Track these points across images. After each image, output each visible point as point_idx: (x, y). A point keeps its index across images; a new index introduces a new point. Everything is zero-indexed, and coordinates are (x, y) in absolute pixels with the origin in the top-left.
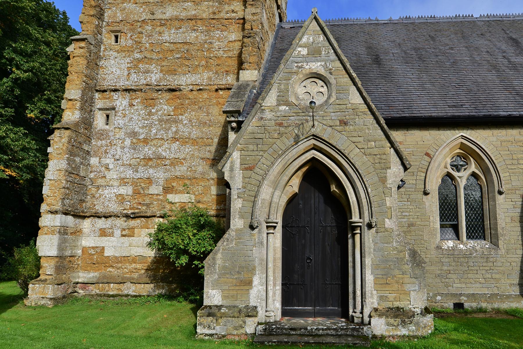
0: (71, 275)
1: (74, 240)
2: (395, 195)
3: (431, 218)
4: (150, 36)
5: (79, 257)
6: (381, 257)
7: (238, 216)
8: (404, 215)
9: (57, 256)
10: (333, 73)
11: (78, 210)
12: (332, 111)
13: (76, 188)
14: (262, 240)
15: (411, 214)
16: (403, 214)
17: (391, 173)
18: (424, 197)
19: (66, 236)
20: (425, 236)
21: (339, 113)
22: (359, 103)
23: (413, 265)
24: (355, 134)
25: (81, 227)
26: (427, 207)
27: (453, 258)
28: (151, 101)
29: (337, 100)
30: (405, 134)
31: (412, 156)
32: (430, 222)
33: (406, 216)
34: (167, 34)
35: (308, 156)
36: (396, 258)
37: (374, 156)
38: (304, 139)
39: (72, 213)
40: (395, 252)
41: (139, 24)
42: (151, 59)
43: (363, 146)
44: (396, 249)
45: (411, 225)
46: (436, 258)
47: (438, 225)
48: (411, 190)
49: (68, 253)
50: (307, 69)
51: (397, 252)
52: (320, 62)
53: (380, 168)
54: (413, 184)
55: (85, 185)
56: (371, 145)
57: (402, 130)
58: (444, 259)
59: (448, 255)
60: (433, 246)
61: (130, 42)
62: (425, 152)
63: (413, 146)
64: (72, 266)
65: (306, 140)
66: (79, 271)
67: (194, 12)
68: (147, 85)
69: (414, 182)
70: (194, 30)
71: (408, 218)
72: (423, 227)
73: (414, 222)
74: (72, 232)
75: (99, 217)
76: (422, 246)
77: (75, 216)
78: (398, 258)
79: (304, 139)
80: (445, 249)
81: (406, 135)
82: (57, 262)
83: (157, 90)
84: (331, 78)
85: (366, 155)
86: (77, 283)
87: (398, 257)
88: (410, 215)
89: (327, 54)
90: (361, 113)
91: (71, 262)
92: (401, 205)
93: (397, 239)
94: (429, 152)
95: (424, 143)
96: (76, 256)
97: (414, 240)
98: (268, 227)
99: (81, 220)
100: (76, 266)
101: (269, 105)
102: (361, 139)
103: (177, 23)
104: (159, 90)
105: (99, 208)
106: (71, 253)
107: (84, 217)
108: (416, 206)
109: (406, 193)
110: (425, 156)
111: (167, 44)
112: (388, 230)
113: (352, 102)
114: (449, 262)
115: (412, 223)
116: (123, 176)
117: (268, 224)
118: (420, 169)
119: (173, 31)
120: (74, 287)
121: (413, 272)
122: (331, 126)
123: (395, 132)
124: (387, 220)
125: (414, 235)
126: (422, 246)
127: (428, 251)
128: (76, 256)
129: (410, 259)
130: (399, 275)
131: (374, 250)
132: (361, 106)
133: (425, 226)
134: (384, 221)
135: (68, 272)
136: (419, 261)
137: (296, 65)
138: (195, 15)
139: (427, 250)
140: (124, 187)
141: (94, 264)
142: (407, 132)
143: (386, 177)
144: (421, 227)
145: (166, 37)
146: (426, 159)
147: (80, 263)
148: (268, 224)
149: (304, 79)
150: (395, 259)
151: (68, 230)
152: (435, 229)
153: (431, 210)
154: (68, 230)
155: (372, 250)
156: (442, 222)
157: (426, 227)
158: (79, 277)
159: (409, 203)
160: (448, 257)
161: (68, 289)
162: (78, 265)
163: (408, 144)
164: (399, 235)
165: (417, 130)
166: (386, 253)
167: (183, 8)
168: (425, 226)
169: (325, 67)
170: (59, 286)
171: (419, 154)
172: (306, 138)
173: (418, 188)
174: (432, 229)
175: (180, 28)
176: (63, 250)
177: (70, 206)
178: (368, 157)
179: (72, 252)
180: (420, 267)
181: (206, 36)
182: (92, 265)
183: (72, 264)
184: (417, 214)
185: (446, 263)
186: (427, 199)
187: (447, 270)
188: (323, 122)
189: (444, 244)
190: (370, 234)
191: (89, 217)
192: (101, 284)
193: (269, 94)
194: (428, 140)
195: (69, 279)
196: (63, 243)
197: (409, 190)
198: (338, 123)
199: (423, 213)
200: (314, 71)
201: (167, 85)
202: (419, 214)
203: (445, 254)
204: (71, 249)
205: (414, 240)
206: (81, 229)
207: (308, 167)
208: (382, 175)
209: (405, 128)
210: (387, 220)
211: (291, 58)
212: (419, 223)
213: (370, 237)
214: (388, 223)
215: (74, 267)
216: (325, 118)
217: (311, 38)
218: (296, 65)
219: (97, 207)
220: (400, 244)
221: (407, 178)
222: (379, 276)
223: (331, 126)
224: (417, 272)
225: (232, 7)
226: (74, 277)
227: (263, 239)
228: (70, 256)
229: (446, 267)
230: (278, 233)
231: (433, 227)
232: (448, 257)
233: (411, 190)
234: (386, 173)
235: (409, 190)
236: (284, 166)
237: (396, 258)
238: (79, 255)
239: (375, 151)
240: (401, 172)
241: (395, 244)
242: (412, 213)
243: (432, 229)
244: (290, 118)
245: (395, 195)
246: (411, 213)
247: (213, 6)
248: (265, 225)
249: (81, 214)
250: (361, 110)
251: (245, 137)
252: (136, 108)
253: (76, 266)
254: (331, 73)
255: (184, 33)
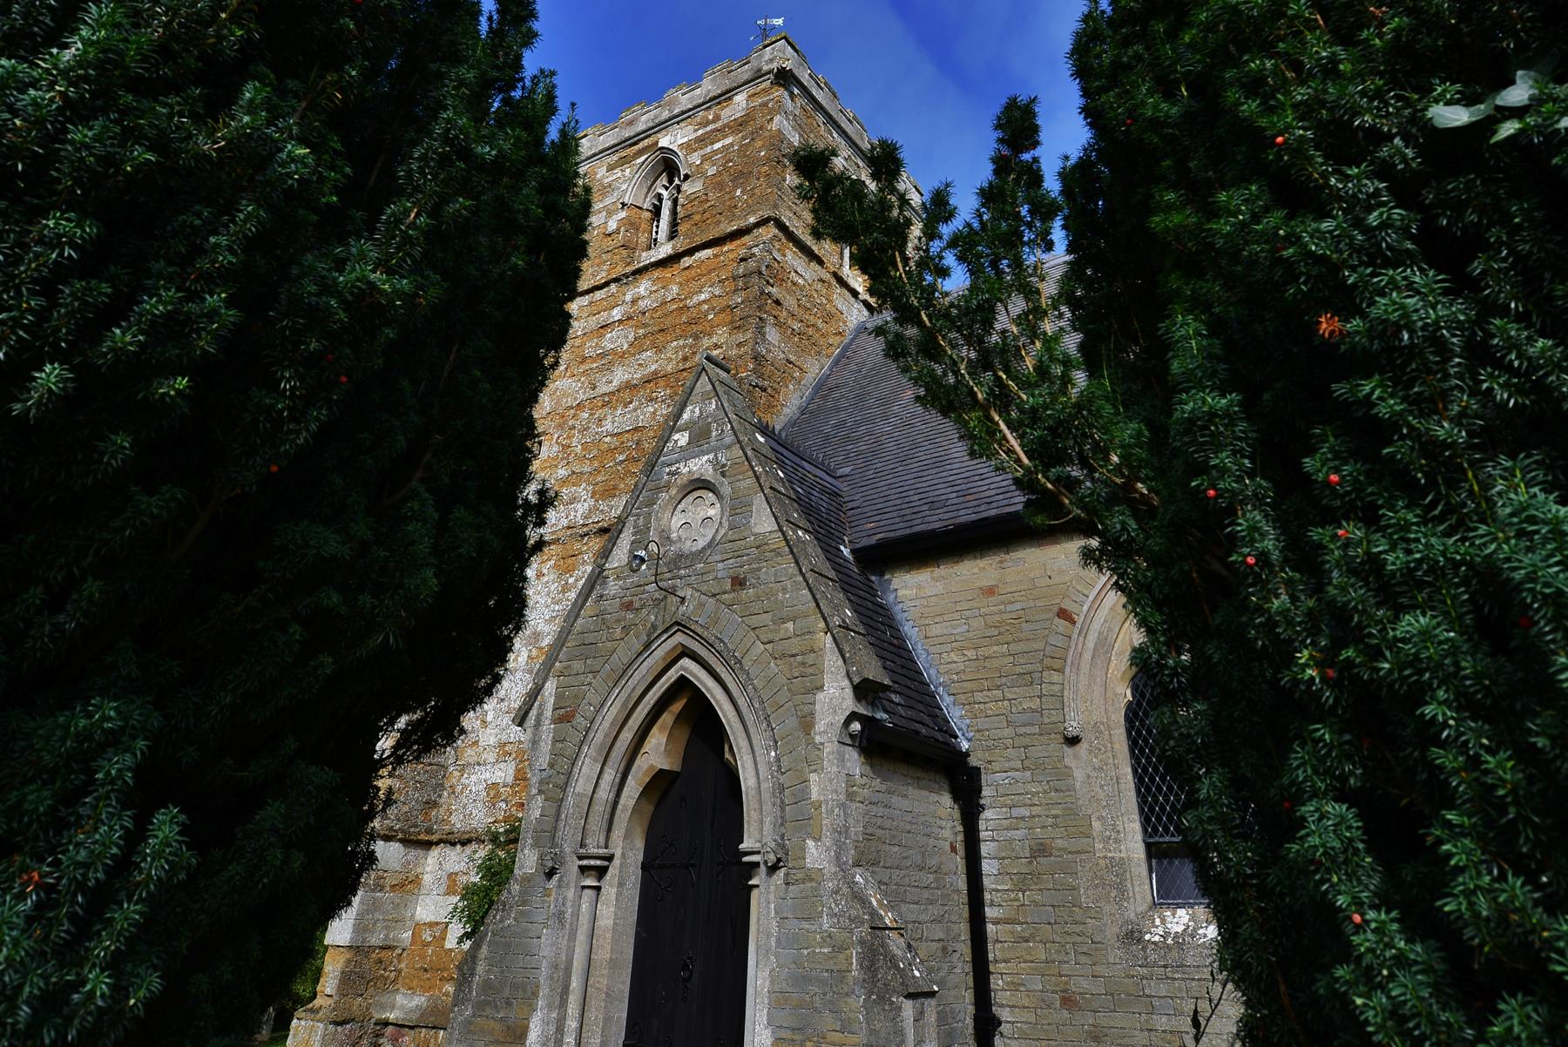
0: (376, 998)
1: (398, 905)
2: (833, 764)
3: (1096, 824)
4: (585, 430)
5: (404, 950)
6: (794, 966)
7: (530, 841)
8: (1016, 818)
9: (351, 947)
10: (727, 474)
11: (416, 826)
12: (718, 558)
13: (419, 774)
14: (562, 909)
15: (1036, 810)
16: (1016, 812)
17: (824, 703)
18: (1068, 750)
19: (378, 894)
20: (1082, 890)
21: (731, 561)
22: (769, 529)
23: (870, 997)
24: (756, 607)
25: (419, 870)
26: (1078, 785)
27: (1183, 979)
28: (569, 561)
29: (730, 532)
30: (1001, 562)
31: (1024, 625)
32: (1093, 839)
33: (1023, 818)
34: (609, 418)
35: (672, 675)
36: (827, 971)
37: (792, 659)
38: (660, 635)
39: (400, 836)
40: (826, 951)
41: (572, 411)
42: (581, 473)
43: (770, 636)
44: (828, 939)
45: (1040, 850)
46: (1127, 980)
47: (1133, 846)
48: (1028, 730)
49: (376, 939)
50: (684, 474)
51: (830, 949)
52: (708, 454)
53: (803, 691)
54: (1034, 711)
55: (443, 766)
56: (787, 630)
57: (995, 554)
58: (1152, 984)
59: (1165, 966)
60: (1112, 931)
61: (555, 449)
62: (1056, 609)
63: (1023, 593)
64: (382, 976)
65: (665, 636)
66: (398, 989)
67: (653, 367)
68: (569, 528)
69: (1035, 704)
70: (651, 400)
71: (1027, 825)
72: (1074, 856)
73: (1048, 841)
74: (396, 882)
75: (453, 844)
76: (1078, 928)
77: (408, 842)
78: (832, 971)
79: (660, 635)
80: (1153, 943)
81: (1004, 565)
82: (349, 961)
83: (581, 536)
84: (722, 483)
85: (776, 658)
86: (386, 1023)
87: (832, 967)
88: (1034, 817)
89: (720, 435)
90: (773, 554)
91: (381, 962)
92: (1006, 781)
93: (833, 905)
94: (1068, 605)
95: (1051, 582)
96: (396, 947)
97: (1053, 906)
98: (583, 869)
99: (421, 852)
100: (393, 974)
101: (616, 565)
102: (767, 619)
103: (626, 395)
104: (585, 535)
105: (457, 822)
106: (384, 940)
107: (428, 845)
108: (1048, 782)
109: (1018, 741)
110: (1057, 621)
111: (607, 439)
112: (813, 876)
113: (756, 530)
114: (1171, 998)
115: (1042, 844)
116: (504, 738)
117: (585, 862)
118: (1047, 661)
119: (619, 412)
120: (377, 1036)
121: (868, 1023)
122: (714, 595)
123: (979, 561)
124: (810, 843)
125: (1051, 886)
126: (1078, 928)
127: (1097, 949)
128: (396, 947)
129: (861, 977)
130: (835, 1033)
131: (778, 941)
132: (773, 536)
133: (1079, 852)
134: (803, 849)
135: (371, 990)
136: (885, 984)
137: (667, 470)
138: (655, 372)
139: (1093, 946)
140: (502, 765)
141: (426, 970)
142: (1007, 557)
143: (812, 714)
144: (1070, 856)
145: (608, 426)
146: (1061, 629)
147: (403, 966)
148: (585, 862)
149: (681, 496)
150: (825, 974)
151: (385, 878)
152: (1119, 867)
153: (1093, 794)
154: (385, 878)
155: (773, 941)
156: (1151, 836)
157: (1083, 857)
158: (393, 1007)
159: (1028, 773)
160: (1167, 978)
161: (360, 1037)
162: (399, 971)
163: (1009, 590)
164: (837, 893)
165: (1031, 547)
166: (805, 952)
167: (639, 365)
168: (1079, 852)
169: (716, 464)
170: (339, 1029)
171: (1042, 617)
172: (665, 631)
173: (1049, 723)
174: (1102, 863)
175: (631, 402)
176: (365, 929)
177: (398, 820)
178: (779, 662)
179: (386, 936)
180: (887, 1007)
181: (668, 406)
182: (421, 973)
183: (385, 969)
184: (1053, 812)
185: (1162, 1001)
186: (1076, 757)
187: (1171, 1032)
188: (702, 589)
189: (1158, 922)
190: (772, 888)
191: (437, 844)
192: (424, 1030)
193: (618, 541)
194: (1061, 572)
195: (368, 1009)
196: (368, 911)
197: (1023, 730)
198: (728, 585)
199: (1068, 805)
200: (696, 476)
201: (598, 522)
202: (1059, 812)
203: (1155, 964)
204: (387, 928)
205: (1053, 906)
206: (417, 876)
207: (685, 700)
208: (806, 709)
209: (1002, 547)
210: (810, 843)
211: (662, 459)
212: (1059, 843)
213: (772, 897)
214: (816, 855)
215: (386, 979)
216: (705, 578)
217: (697, 409)
218: (667, 470)
219: (453, 819)
220: (839, 922)
221: (1016, 693)
222: (783, 1035)
223: (714, 595)
224: (878, 1027)
225: (714, 340)
226: (383, 1007)
227: (563, 905)
228: (381, 948)
229: (1164, 1019)
230: (611, 885)
231: (1105, 857)
232: (1167, 978)
233: (1028, 730)
234: (814, 704)
235: (1023, 730)
236: (624, 705)
237: (827, 971)
238: (404, 946)
239: (794, 645)
240: (846, 697)
241: (826, 922)
242: (1039, 808)
243: (1102, 863)
244: (646, 587)
245: (833, 764)
246: (1035, 808)
247: (684, 346)
248: (573, 865)
249: (423, 837)
250: (772, 547)
251: (569, 644)
252: (546, 579)
253: (393, 974)
254: (723, 474)
255: (635, 410)
